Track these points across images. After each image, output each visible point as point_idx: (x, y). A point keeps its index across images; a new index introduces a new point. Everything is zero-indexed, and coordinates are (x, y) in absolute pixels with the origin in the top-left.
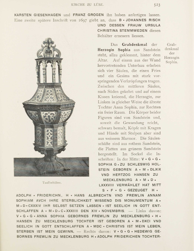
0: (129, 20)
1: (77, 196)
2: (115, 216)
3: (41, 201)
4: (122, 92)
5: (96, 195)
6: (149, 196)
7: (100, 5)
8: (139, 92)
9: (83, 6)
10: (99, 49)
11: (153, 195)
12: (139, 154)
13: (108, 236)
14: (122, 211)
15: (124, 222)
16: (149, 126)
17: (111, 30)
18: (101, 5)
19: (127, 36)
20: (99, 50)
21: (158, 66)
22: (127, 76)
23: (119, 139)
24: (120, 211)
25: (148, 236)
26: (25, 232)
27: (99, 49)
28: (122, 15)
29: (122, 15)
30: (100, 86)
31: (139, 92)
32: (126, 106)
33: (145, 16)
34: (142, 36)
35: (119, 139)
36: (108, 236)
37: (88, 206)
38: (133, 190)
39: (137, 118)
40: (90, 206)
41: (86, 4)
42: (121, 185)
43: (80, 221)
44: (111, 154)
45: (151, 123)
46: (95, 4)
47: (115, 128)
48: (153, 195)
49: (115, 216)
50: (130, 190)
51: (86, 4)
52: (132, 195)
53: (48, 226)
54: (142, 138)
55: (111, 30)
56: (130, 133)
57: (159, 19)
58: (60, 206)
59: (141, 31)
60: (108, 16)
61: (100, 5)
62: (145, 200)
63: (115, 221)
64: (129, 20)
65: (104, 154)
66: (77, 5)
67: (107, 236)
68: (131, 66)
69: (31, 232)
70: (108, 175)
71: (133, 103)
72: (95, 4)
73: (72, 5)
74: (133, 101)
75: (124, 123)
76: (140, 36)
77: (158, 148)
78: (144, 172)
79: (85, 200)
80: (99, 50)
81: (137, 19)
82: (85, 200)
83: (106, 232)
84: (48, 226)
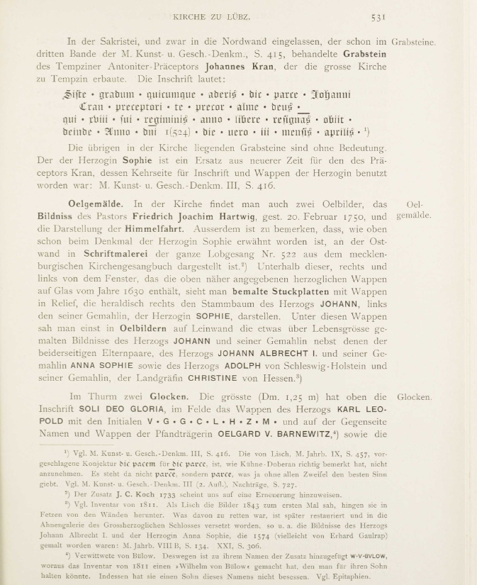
0: (328, 304)
1: (192, 342)
5: (278, 353)
7: (240, 17)
8: (224, 342)
9: (200, 21)
10: (223, 215)
12: (305, 230)
13: (251, 364)
14: (211, 378)
17: (221, 378)
18: (244, 17)
19: (122, 354)
20: (223, 218)
21: (48, 354)
23: (238, 230)
24: (207, 378)
26: (251, 435)
27: (223, 215)
28: (329, 330)
29: (329, 330)
31: (224, 342)
32: (287, 364)
35: (238, 230)
36: (251, 364)
39: (222, 330)
41: (208, 17)
45: (47, 379)
46: (231, 17)
47: (71, 242)
51: (208, 17)
52: (284, 354)
54: (142, 78)
55: (221, 378)
56: (206, 303)
60: (117, 135)
61: (240, 17)
62: (217, 378)
64: (328, 304)
66: (187, 17)
67: (247, 365)
70: (258, 434)
71: (356, 281)
72: (231, 17)
73: (175, 17)
75: (270, 341)
77: (162, 171)
78: (178, 114)
80: (223, 218)
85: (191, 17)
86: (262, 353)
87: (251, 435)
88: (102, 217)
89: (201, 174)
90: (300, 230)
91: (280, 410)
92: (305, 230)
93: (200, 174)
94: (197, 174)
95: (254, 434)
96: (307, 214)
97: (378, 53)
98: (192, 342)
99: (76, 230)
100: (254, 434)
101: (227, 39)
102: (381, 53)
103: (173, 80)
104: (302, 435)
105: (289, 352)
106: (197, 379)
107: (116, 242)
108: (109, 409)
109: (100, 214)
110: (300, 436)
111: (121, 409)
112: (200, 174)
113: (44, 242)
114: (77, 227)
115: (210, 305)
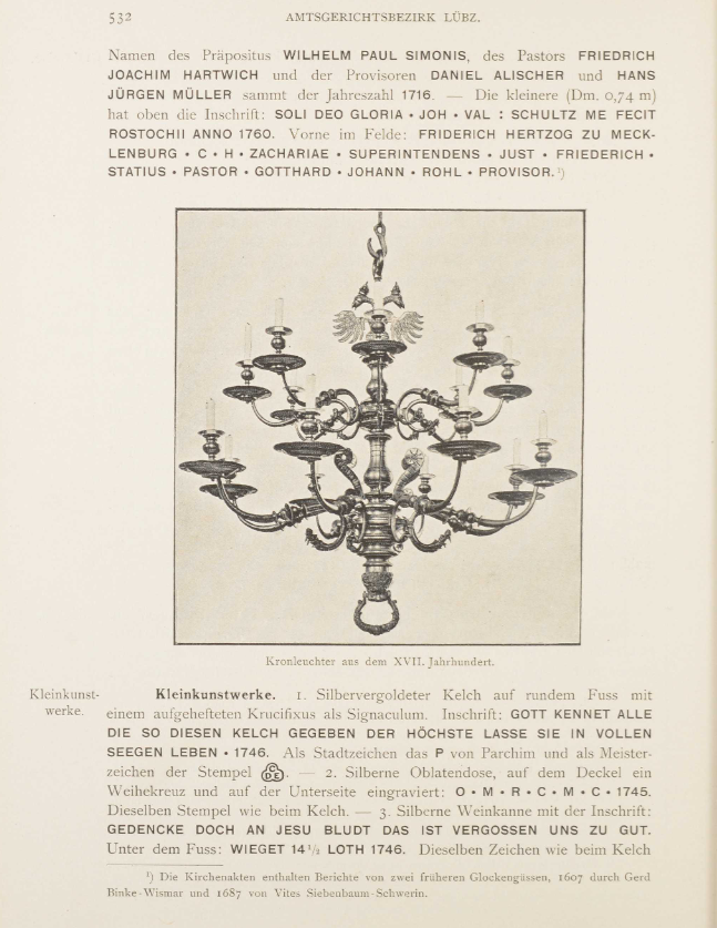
1: (302, 172)
2: (597, 829)
3: (604, 735)
4: (181, 717)
6: (250, 830)
7: (465, 17)
11: (397, 169)
15: (535, 832)
16: (617, 843)
18: (470, 17)
19: (435, 813)
22: (136, 57)
25: (220, 830)
26: (316, 174)
30: (496, 850)
33: (151, 778)
34: (419, 894)
37: (490, 734)
38: (405, 17)
40: (496, 734)
42: (470, 829)
43: (151, 134)
44: (634, 755)
46: (450, 17)
47: (274, 812)
48: (209, 137)
49: (597, 829)
50: (117, 828)
53: (347, 848)
56: (322, 751)
57: (360, 847)
58: (509, 75)
59: (595, 154)
63: (495, 830)
65: (375, 697)
68: (300, 794)
69: (145, 831)
70: (327, 172)
72: (450, 17)
74: (462, 808)
76: (475, 662)
79: (240, 733)
81: (258, 827)
82: (240, 733)
83: (462, 755)
84: (532, 713)
85: (358, 17)
86: (621, 715)
87: (316, 174)
88: (490, 754)
89: (452, 716)
90: (66, 712)
91: (170, 773)
92: (73, 712)
93: (452, 716)
94: (447, 716)
95: (321, 172)
96: (593, 692)
97: (179, 692)
98: (302, 172)
99: (634, 755)
100: (321, 172)
101: (116, 53)
102: (183, 692)
103: (466, 716)
104: (593, 715)
105: (333, 113)
106: (254, 77)
107: (158, 793)
108: (319, 114)
109: (486, 750)
110: (134, 156)
111: (338, 114)
112: (452, 716)
113: (599, 774)
114: (635, 751)
115: (327, 754)
